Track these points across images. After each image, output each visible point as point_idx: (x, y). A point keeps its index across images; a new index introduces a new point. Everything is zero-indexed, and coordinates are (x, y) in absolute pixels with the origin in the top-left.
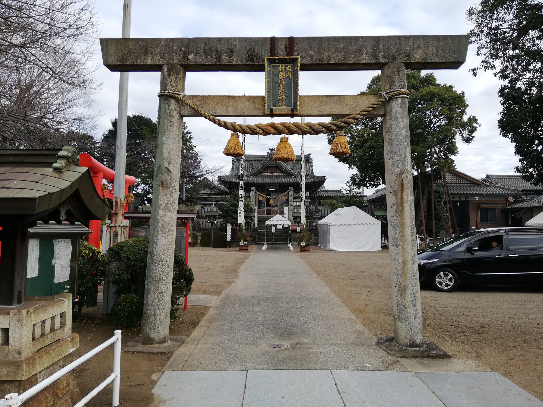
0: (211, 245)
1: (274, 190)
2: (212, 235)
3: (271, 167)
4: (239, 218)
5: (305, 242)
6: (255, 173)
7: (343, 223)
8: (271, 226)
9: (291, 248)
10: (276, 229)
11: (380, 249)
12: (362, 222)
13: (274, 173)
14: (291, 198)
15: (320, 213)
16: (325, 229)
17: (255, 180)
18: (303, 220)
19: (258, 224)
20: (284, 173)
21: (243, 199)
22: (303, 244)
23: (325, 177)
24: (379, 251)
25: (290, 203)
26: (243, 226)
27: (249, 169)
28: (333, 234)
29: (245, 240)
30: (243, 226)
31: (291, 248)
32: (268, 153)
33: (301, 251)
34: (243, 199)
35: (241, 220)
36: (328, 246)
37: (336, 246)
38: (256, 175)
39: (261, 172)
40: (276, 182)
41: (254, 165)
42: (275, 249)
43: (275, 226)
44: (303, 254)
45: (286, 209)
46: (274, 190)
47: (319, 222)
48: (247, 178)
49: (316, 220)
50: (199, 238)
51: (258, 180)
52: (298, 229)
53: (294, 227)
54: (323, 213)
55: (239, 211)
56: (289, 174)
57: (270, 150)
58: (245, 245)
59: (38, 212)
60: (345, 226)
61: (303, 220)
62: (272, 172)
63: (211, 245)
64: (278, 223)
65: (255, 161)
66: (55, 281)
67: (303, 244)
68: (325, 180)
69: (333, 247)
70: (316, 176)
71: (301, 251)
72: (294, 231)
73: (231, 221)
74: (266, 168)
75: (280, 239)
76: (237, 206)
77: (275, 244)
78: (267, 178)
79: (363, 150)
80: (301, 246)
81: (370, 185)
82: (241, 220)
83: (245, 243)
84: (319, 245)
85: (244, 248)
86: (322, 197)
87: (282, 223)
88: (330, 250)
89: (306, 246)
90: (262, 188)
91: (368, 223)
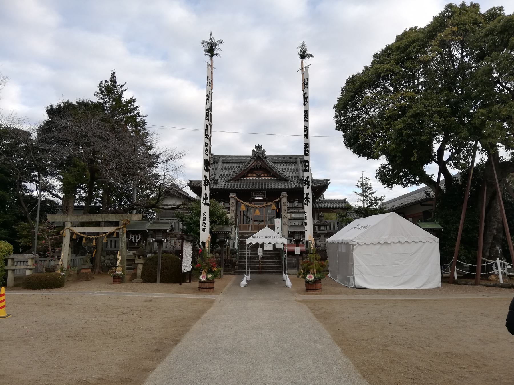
0: (158, 279)
1: (261, 198)
2: (160, 262)
3: (257, 169)
4: (202, 234)
5: (313, 274)
6: (236, 177)
7: (376, 241)
8: (257, 245)
9: (289, 283)
10: (264, 251)
11: (440, 285)
12: (406, 239)
13: (261, 177)
14: (284, 208)
15: (328, 227)
16: (343, 249)
17: (237, 186)
18: (309, 235)
19: (238, 246)
20: (273, 176)
21: (208, 201)
22: (310, 277)
23: (328, 180)
24: (438, 288)
25: (283, 214)
26: (208, 246)
27: (229, 173)
28: (359, 259)
29: (210, 271)
30: (208, 246)
31: (289, 283)
32: (253, 151)
33: (307, 290)
34: (208, 201)
35: (205, 236)
36: (351, 280)
37: (365, 281)
38: (238, 180)
39: (244, 176)
40: (264, 187)
41: (236, 167)
42: (263, 283)
43: (262, 245)
44: (311, 297)
45: (277, 222)
46: (261, 198)
47: (330, 240)
48: (226, 184)
49: (322, 237)
50: (140, 267)
51: (240, 185)
52: (298, 251)
53: (291, 248)
54: (332, 227)
55: (202, 222)
56: (281, 178)
57: (256, 147)
58: (208, 281)
59: (184, 244)
60: (378, 246)
61: (309, 235)
62: (258, 176)
63: (158, 279)
64: (266, 241)
65: (237, 163)
66: (183, 270)
67: (310, 277)
68: (328, 184)
69: (359, 282)
70: (317, 180)
71: (307, 290)
72: (291, 253)
73: (191, 239)
74: (251, 170)
75: (270, 266)
76: (198, 214)
77: (262, 273)
78: (252, 182)
79: (404, 121)
80: (307, 282)
81: (408, 183)
82: (205, 236)
83: (210, 276)
84: (329, 275)
85: (207, 285)
86: (322, 208)
87: (273, 241)
88: (355, 287)
89: (317, 281)
90: (245, 195)
91: (417, 240)
